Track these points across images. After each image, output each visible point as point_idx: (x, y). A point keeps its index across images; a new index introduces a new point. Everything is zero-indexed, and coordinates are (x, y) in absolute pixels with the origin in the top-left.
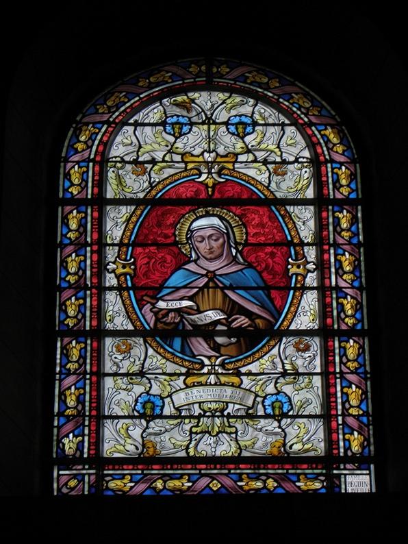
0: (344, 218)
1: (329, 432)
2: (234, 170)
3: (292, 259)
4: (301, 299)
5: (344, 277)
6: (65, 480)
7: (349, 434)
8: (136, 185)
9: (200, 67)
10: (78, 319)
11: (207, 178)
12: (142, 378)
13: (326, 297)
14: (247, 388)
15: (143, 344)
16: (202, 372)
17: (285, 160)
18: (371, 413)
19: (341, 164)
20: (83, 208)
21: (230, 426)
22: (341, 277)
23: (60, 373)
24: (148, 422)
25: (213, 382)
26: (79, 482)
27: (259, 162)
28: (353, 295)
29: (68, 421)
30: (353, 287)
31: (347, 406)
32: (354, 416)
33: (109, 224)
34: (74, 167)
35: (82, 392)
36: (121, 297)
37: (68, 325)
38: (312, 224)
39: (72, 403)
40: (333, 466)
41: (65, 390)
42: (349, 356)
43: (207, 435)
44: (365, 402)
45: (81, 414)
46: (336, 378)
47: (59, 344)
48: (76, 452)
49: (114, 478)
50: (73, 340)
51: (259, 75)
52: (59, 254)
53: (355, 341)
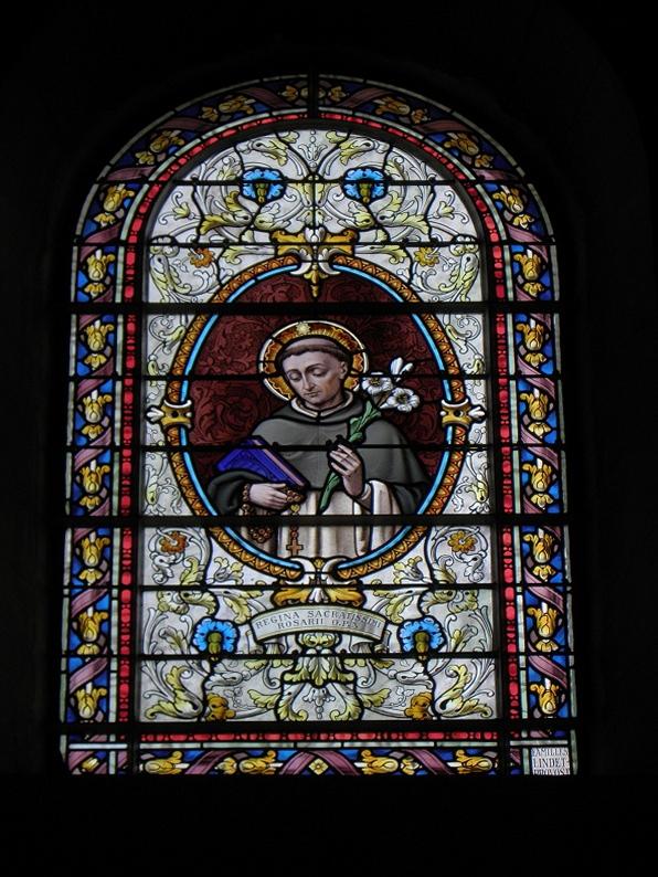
5: (534, 499)
6: (82, 755)
7: (533, 606)
8: (199, 282)
9: (299, 90)
16: (300, 583)
19: (526, 245)
22: (523, 358)
25: (317, 600)
29: (85, 664)
32: (545, 654)
33: (152, 344)
38: (479, 342)
46: (516, 594)
47: (69, 536)
50: (91, 532)
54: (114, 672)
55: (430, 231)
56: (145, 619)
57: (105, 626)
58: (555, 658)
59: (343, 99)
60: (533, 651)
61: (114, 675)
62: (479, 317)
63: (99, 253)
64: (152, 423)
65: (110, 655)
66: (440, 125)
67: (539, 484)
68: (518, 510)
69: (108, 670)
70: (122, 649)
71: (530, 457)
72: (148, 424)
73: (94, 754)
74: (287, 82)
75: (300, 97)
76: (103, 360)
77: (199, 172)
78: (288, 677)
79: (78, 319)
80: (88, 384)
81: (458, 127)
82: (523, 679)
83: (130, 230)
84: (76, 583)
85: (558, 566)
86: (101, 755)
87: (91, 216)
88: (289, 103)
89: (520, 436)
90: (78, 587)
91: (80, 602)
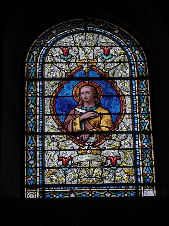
11: (86, 69)
40: (44, 188)
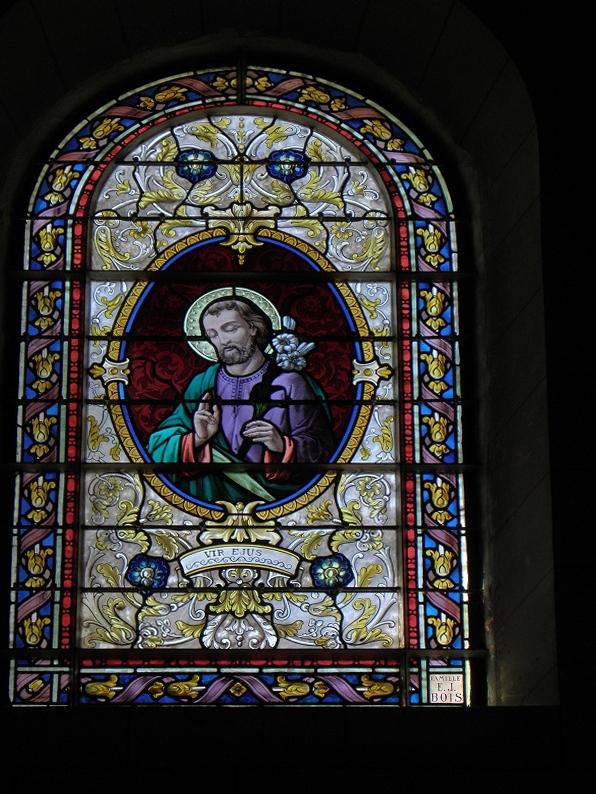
0: (434, 299)
1: (409, 614)
2: (276, 229)
3: (358, 361)
4: (370, 417)
5: (432, 449)
6: (23, 681)
7: (431, 549)
8: (138, 251)
9: (229, 81)
10: (44, 578)
12: (137, 532)
13: (406, 445)
14: (290, 548)
15: (140, 484)
16: (225, 524)
17: (350, 214)
18: (466, 588)
19: (428, 221)
20: (59, 285)
21: (263, 604)
22: (424, 258)
23: (19, 526)
24: (145, 598)
26: (45, 684)
27: (313, 218)
28: (440, 348)
29: (32, 595)
30: (439, 336)
31: (431, 575)
32: (441, 591)
33: (94, 307)
34: (45, 227)
35: (53, 485)
36: (110, 411)
37: (35, 454)
38: (387, 311)
39: (47, 245)
41: (23, 621)
42: (435, 503)
43: (230, 617)
44: (451, 372)
45: (48, 586)
46: (417, 535)
47: (18, 480)
48: (41, 642)
49: (95, 678)
50: (39, 476)
51: (317, 92)
52: (12, 616)
53: (444, 481)
54: (57, 603)
55: (345, 207)
56: (86, 555)
57: (58, 365)
58: (451, 595)
59: (268, 89)
60: (431, 587)
61: (57, 606)
62: (387, 286)
63: (49, 226)
64: (94, 379)
65: (54, 587)
66: (357, 113)
67: (440, 435)
68: (418, 460)
69: (52, 601)
70: (66, 582)
71: (428, 349)
72: (90, 379)
73: (40, 675)
74: (217, 74)
75: (230, 86)
76: (54, 258)
77: (139, 152)
78: (211, 608)
79: (29, 286)
80: (32, 408)
81: (371, 113)
82: (420, 545)
83: (78, 205)
84: (24, 523)
85: (454, 513)
86: (46, 677)
87: (41, 197)
88: (218, 91)
89: (420, 393)
90: (24, 527)
91: (28, 540)
